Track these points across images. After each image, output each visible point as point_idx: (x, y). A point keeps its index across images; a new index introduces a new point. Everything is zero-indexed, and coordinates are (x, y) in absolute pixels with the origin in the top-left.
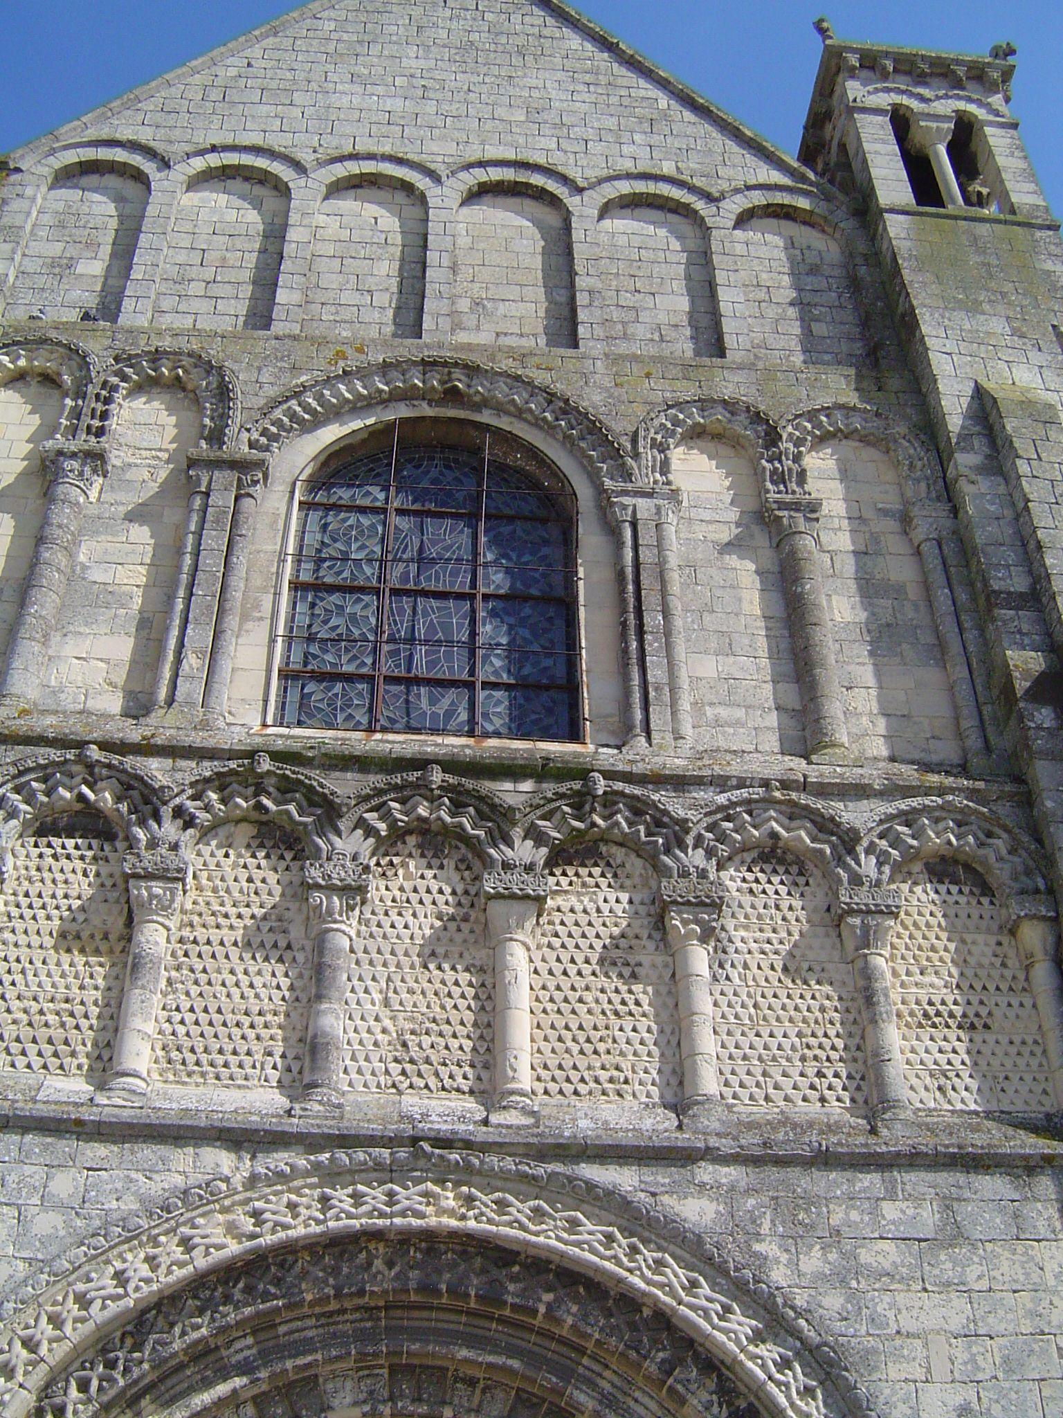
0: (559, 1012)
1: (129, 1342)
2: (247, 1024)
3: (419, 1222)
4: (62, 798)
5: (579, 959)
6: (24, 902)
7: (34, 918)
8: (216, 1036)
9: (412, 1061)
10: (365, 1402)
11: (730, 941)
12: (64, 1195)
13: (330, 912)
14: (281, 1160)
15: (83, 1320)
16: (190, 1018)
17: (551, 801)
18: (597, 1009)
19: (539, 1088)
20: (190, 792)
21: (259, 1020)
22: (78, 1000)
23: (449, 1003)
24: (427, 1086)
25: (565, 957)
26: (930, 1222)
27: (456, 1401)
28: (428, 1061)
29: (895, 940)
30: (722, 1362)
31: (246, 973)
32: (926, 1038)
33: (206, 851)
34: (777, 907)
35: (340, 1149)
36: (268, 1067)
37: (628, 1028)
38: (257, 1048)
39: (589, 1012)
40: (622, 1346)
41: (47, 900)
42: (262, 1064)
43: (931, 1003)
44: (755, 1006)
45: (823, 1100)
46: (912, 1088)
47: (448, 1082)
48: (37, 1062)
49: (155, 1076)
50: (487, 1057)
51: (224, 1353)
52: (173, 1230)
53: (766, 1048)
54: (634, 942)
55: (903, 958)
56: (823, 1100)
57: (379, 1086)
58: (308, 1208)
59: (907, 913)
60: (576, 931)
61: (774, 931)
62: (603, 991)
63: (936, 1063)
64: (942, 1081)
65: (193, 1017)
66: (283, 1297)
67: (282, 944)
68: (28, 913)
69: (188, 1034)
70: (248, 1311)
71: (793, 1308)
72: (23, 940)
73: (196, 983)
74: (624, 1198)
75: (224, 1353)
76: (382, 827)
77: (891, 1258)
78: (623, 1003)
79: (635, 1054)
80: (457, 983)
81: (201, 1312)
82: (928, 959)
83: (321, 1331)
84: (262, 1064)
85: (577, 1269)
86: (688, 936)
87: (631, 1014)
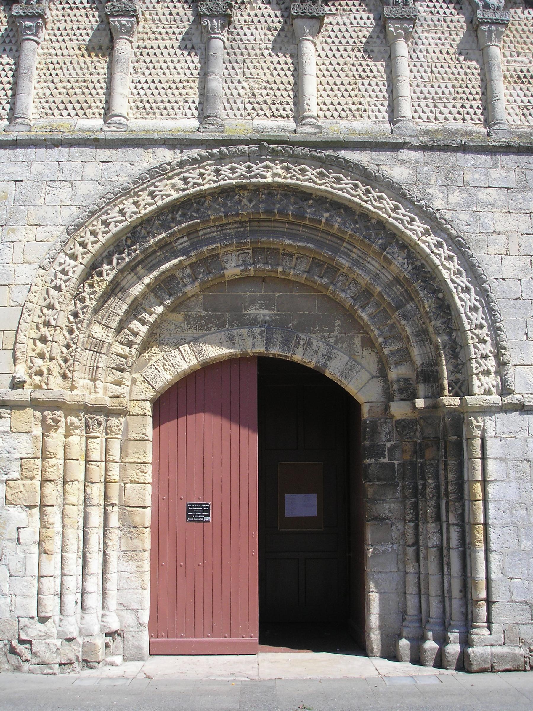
0: (331, 76)
2: (174, 87)
3: (264, 180)
5: (342, 48)
6: (58, 33)
7: (64, 41)
8: (159, 94)
9: (258, 103)
10: (241, 265)
12: (92, 175)
13: (213, 29)
14: (194, 153)
15: (106, 233)
16: (146, 86)
18: (350, 74)
19: (321, 114)
21: (180, 85)
22: (90, 80)
23: (275, 73)
24: (265, 115)
25: (334, 48)
26: (514, 180)
27: (284, 264)
28: (265, 102)
29: (505, 38)
30: (410, 244)
32: (518, 89)
34: (445, 21)
35: (223, 148)
36: (186, 108)
37: (366, 83)
38: (179, 98)
43: (522, 71)
45: (464, 119)
46: (509, 114)
47: (276, 113)
48: (73, 113)
49: (131, 115)
51: (174, 245)
53: (436, 93)
55: (509, 47)
56: (464, 119)
57: (241, 115)
58: (209, 175)
59: (513, 24)
60: (340, 35)
61: (443, 33)
62: (353, 65)
63: (522, 102)
64: (525, 111)
65: (151, 92)
66: (200, 218)
67: (189, 46)
68: (60, 39)
69: (145, 94)
70: (184, 225)
71: (445, 220)
72: (59, 52)
73: (148, 68)
74: (363, 167)
75: (174, 245)
77: (493, 197)
78: (364, 71)
79: (370, 96)
80: (279, 63)
82: (522, 48)
83: (219, 233)
85: (340, 201)
86: (399, 36)
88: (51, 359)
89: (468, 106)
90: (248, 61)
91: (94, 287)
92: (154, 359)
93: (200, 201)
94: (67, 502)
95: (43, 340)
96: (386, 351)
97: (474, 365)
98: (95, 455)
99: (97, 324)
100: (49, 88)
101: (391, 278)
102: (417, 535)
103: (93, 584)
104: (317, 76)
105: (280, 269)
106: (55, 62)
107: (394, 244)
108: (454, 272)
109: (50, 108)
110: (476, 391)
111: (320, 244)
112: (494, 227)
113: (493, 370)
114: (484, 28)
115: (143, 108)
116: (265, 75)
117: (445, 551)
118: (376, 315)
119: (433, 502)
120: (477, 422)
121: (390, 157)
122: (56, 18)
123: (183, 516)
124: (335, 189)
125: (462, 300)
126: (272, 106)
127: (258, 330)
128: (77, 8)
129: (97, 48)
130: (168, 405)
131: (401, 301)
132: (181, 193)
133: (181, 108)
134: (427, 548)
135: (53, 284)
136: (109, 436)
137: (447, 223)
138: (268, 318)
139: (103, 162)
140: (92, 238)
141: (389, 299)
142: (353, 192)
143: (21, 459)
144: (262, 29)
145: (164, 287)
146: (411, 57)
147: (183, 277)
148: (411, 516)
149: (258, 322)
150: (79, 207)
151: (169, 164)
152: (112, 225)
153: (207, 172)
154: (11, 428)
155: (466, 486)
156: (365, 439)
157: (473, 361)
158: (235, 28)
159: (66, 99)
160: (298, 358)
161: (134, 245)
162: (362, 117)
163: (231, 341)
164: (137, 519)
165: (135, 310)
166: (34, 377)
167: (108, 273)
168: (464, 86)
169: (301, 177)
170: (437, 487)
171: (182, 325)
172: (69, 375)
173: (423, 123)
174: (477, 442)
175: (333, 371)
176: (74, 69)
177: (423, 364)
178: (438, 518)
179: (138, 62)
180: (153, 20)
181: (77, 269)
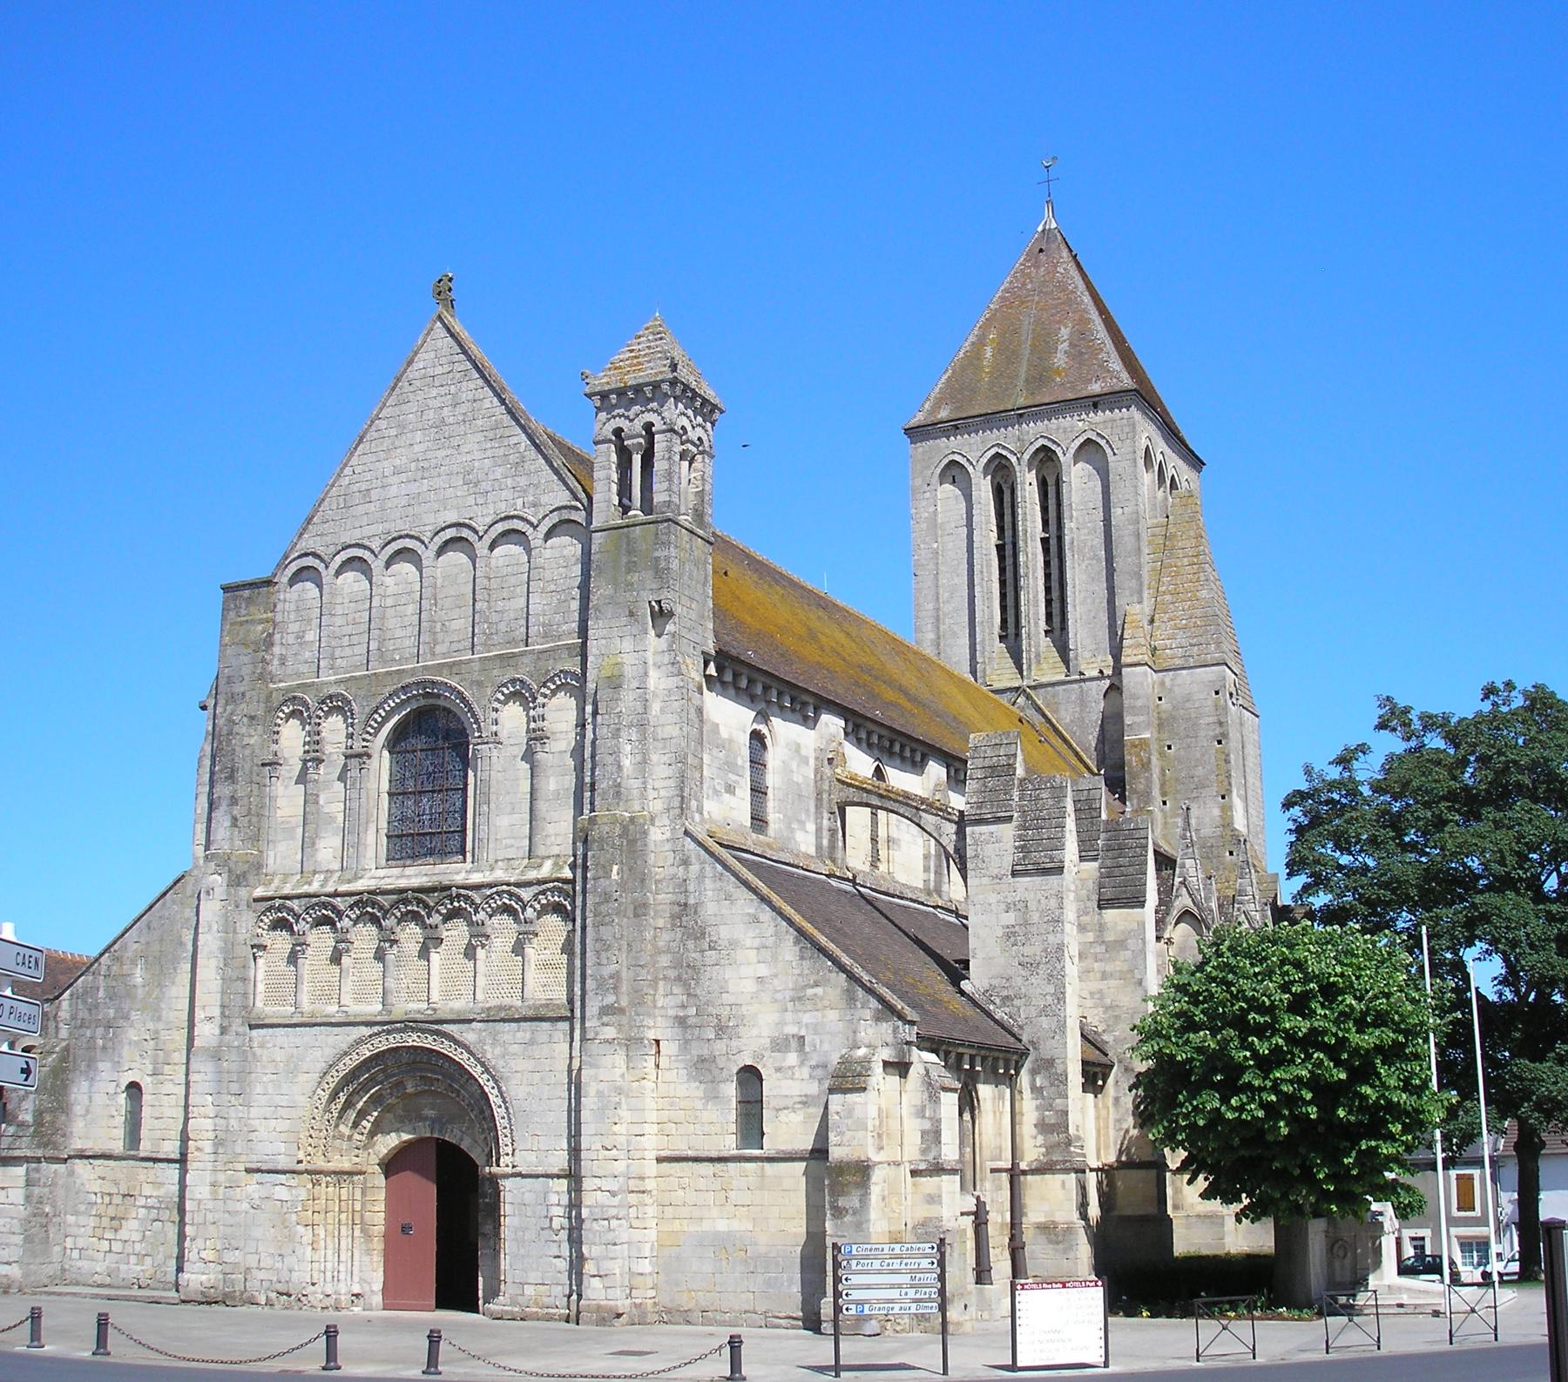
14: (376, 1029)
123: (398, 1232)
130: (391, 1165)
145: (376, 1101)
163: (414, 1131)
165: (362, 1114)
167: (342, 1097)
181: (325, 1096)
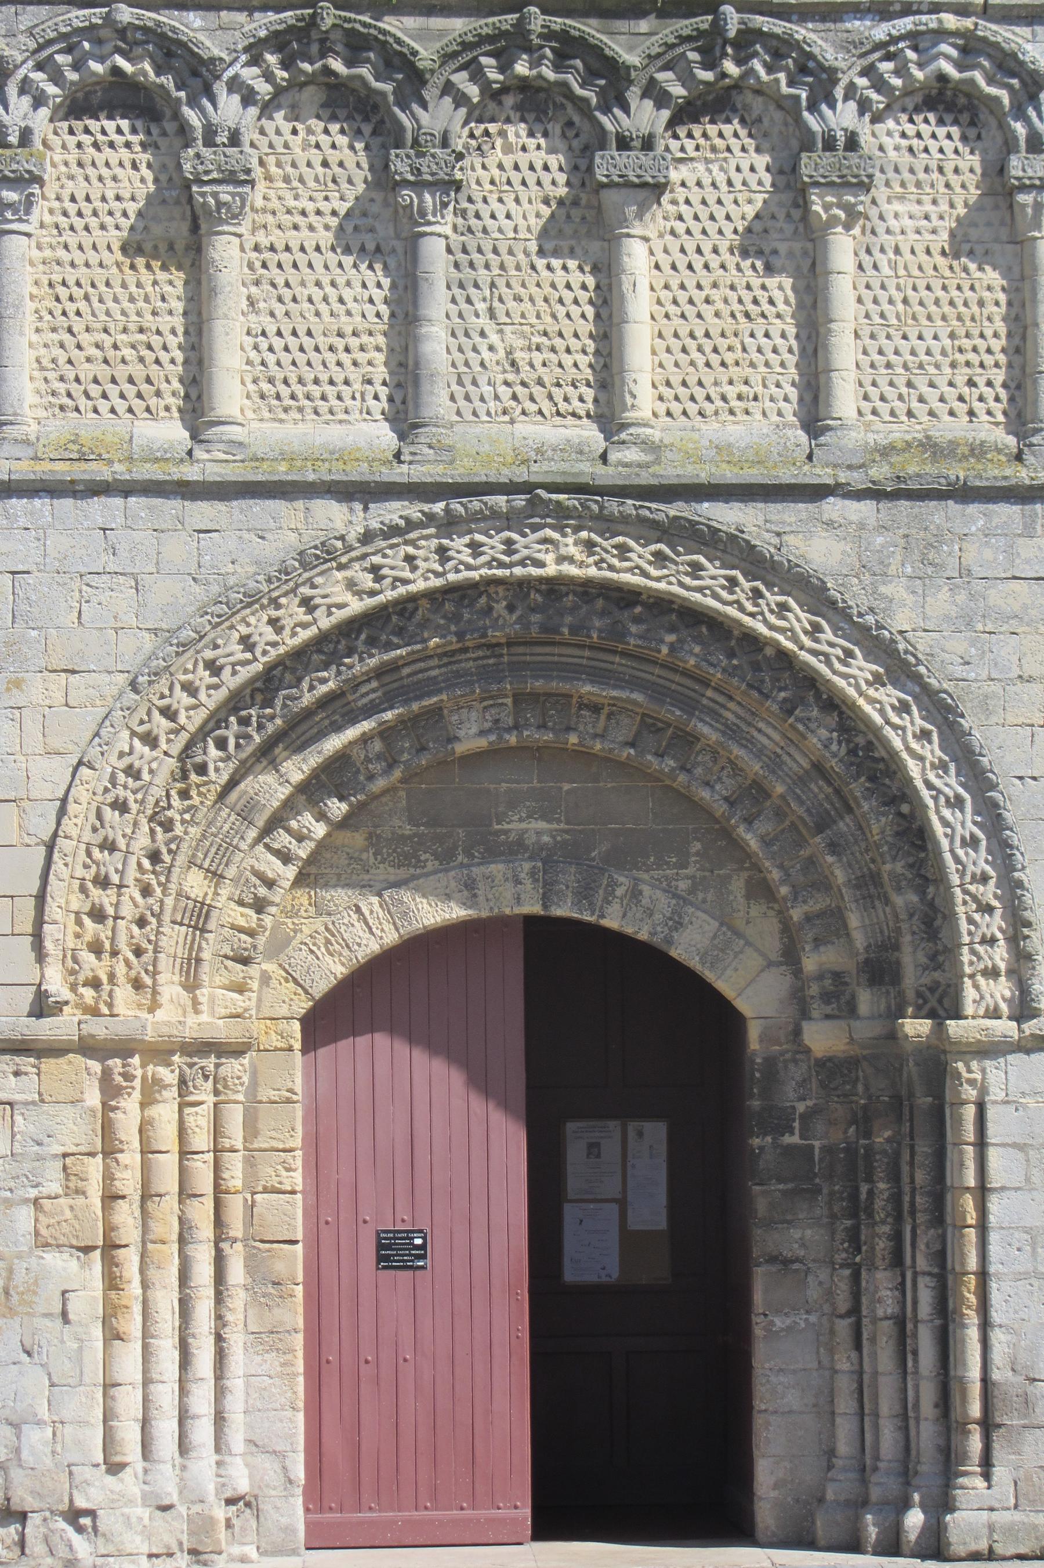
1: (259, 697)
2: (341, 348)
4: (94, 74)
6: (72, 209)
8: (309, 364)
10: (489, 731)
11: (881, 218)
13: (423, 213)
14: (394, 512)
15: (216, 687)
16: (278, 343)
17: (673, 46)
18: (725, 311)
20: (244, 58)
21: (354, 342)
23: (561, 311)
24: (540, 412)
27: (581, 728)
28: (540, 382)
31: (333, 284)
33: (269, 126)
34: (941, 170)
35: (457, 501)
36: (369, 398)
37: (759, 334)
38: (355, 375)
39: (717, 315)
40: (744, 686)
41: (98, 204)
42: (363, 394)
44: (905, 301)
45: (971, 413)
47: (563, 406)
48: (121, 406)
49: (250, 414)
50: (604, 375)
51: (350, 698)
52: (294, 591)
54: (770, 224)
57: (488, 414)
58: (426, 560)
61: (934, 202)
62: (732, 288)
67: (371, 246)
70: (373, 662)
72: (79, 257)
76: (473, 91)
79: (767, 364)
81: (326, 667)
84: (363, 394)
86: (833, 221)
87: (763, 315)
88: (114, 953)
89: (981, 381)
90: (501, 283)
91: (190, 798)
92: (306, 930)
93: (404, 609)
94: (152, 1237)
95: (98, 915)
96: (796, 914)
97: (966, 956)
98: (201, 1140)
99: (195, 869)
100: (62, 346)
101: (805, 764)
102: (856, 1295)
103: (202, 1400)
104: (653, 318)
105: (573, 739)
106: (71, 282)
107: (811, 699)
108: (932, 764)
109: (69, 395)
110: (969, 1009)
111: (658, 693)
112: (1020, 666)
113: (1002, 966)
114: (1022, 198)
115: (276, 396)
116: (538, 317)
117: (910, 1326)
118: (776, 838)
119: (886, 1229)
120: (969, 1071)
121: (804, 515)
122: (63, 169)
124: (688, 588)
125: (946, 823)
126: (555, 390)
127: (527, 866)
128: (112, 145)
129: (163, 247)
130: (328, 1021)
131: (828, 813)
132: (370, 602)
133: (358, 395)
134: (875, 1320)
135: (110, 798)
136: (222, 1098)
137: (919, 662)
138: (546, 839)
139: (200, 531)
140: (186, 700)
141: (801, 811)
142: (724, 594)
143: (65, 1155)
144: (530, 202)
146: (860, 267)
147: (368, 760)
148: (844, 1255)
149: (526, 849)
150: (155, 631)
151: (342, 538)
152: (227, 672)
153: (421, 553)
154: (40, 1094)
155: (949, 1197)
156: (752, 1096)
157: (965, 950)
158: (470, 200)
159: (103, 372)
160: (611, 922)
161: (269, 706)
162: (747, 413)
163: (469, 890)
164: (280, 1268)
166: (82, 990)
168: (976, 332)
169: (615, 562)
170: (896, 1198)
171: (364, 856)
172: (148, 980)
173: (880, 426)
174: (970, 1112)
175: (688, 948)
176: (116, 300)
177: (869, 946)
178: (897, 1260)
179: (257, 283)
180: (287, 179)
